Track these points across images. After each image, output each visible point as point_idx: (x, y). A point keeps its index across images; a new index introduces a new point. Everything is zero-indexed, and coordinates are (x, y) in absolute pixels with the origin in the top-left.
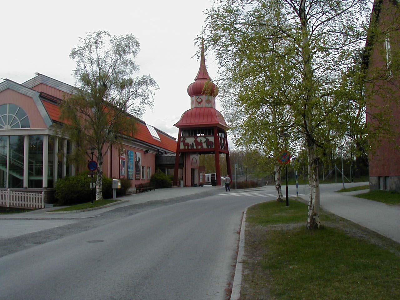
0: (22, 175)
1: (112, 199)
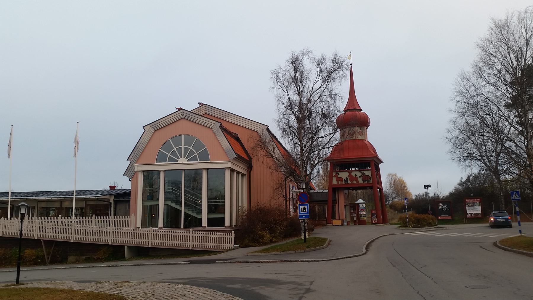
0: (200, 212)
1: (300, 238)
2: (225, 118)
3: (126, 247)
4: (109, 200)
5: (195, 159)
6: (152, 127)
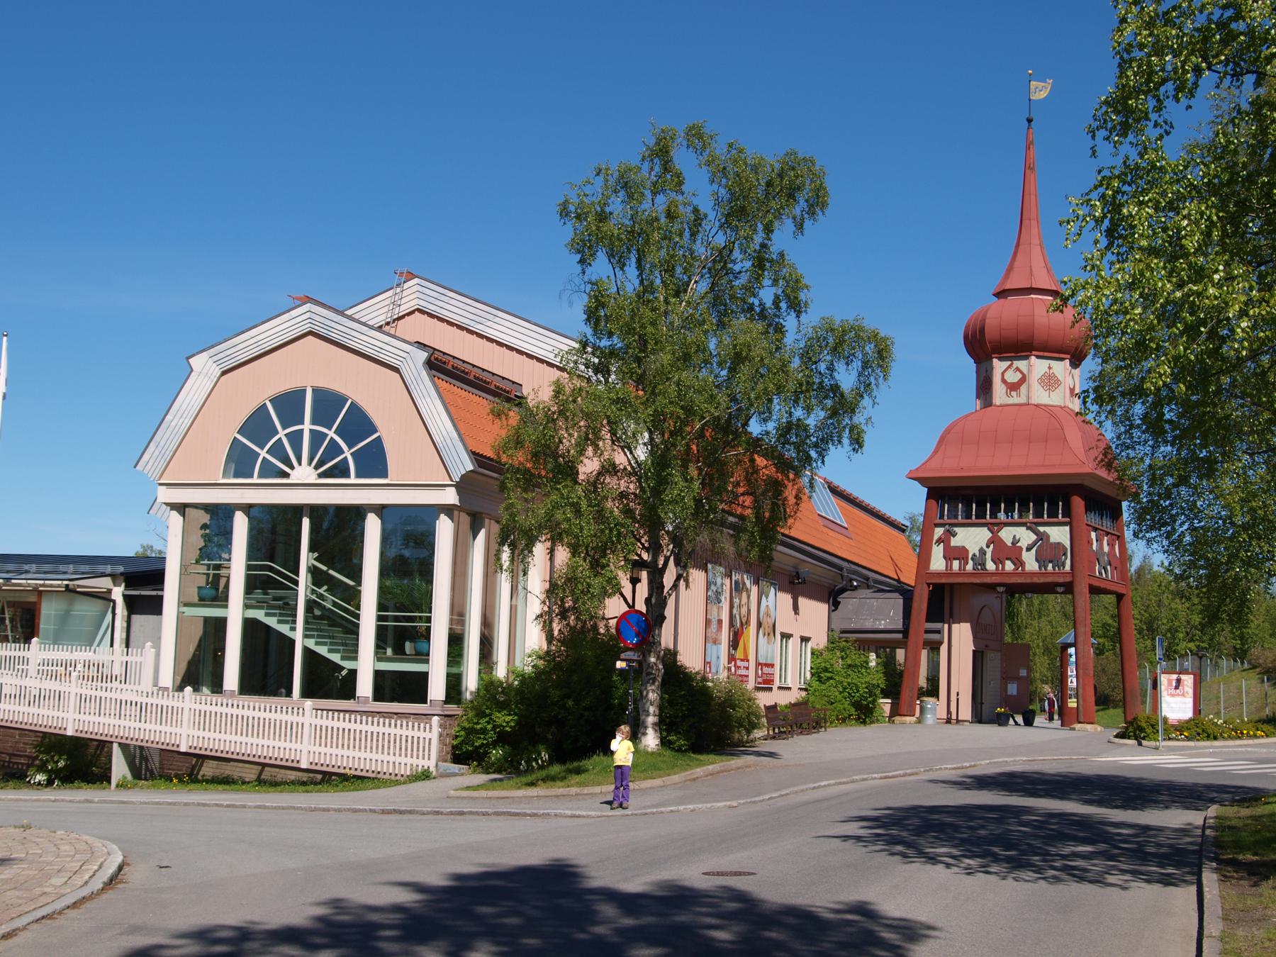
2: (480, 327)
3: (115, 746)
4: (110, 591)
5: (341, 470)
6: (215, 358)
